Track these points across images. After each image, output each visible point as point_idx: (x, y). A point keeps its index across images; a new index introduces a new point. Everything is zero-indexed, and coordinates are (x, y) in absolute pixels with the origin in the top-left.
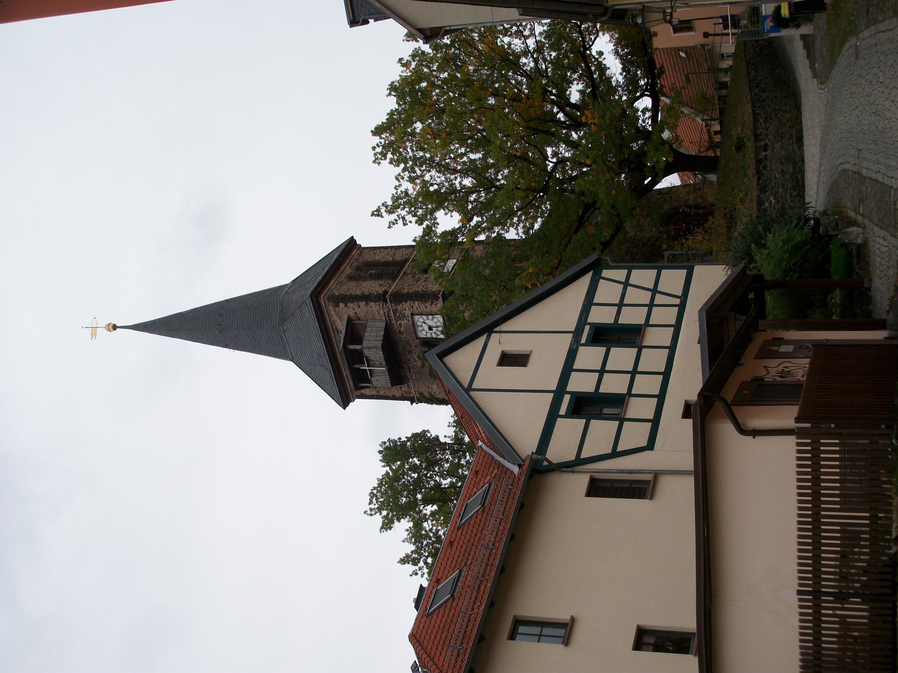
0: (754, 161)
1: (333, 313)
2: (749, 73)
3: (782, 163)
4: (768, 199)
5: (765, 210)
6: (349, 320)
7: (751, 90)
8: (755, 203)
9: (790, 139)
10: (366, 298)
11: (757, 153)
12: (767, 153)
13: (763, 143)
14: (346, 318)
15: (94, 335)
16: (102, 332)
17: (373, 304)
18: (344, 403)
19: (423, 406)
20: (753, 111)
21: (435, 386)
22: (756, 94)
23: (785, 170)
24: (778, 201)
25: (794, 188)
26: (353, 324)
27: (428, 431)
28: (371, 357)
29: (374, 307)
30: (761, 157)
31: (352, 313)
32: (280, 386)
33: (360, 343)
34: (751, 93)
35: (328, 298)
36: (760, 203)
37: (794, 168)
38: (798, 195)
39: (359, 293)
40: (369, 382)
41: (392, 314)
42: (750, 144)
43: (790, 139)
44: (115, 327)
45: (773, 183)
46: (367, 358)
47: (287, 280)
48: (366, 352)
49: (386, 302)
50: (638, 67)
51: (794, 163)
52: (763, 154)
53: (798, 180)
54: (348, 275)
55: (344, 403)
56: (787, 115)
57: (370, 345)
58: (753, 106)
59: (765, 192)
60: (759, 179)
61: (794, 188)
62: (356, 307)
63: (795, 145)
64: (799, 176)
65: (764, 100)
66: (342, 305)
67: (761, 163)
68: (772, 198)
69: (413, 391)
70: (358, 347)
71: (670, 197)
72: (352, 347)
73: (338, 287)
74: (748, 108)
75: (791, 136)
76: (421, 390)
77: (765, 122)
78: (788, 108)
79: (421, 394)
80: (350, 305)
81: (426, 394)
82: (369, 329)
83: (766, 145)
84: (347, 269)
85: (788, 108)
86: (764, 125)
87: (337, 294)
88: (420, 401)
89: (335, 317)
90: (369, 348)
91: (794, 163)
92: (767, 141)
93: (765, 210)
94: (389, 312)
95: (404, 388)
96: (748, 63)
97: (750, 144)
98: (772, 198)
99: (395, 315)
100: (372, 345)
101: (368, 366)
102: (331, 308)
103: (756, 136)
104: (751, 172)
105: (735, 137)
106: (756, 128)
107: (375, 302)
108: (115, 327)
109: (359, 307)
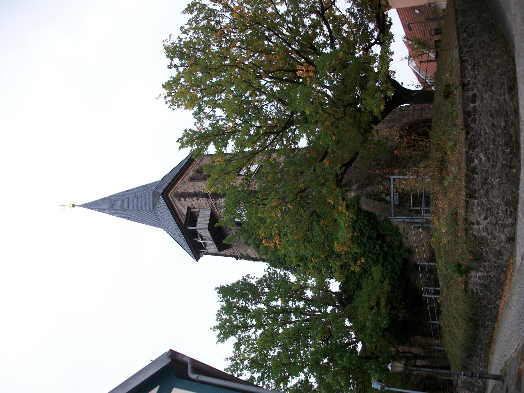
0: (462, 114)
1: (178, 204)
2: (457, 19)
3: (492, 115)
4: (478, 156)
5: (475, 168)
6: (189, 208)
7: (458, 35)
8: (464, 157)
9: (500, 89)
10: (197, 195)
11: (465, 105)
12: (476, 104)
13: (471, 93)
17: (201, 199)
20: (461, 58)
21: (249, 250)
22: (464, 39)
24: (488, 158)
25: (507, 144)
26: (192, 212)
28: (203, 235)
31: (190, 205)
32: (159, 243)
33: (195, 225)
34: (458, 38)
35: (174, 195)
36: (469, 160)
37: (506, 122)
38: (511, 152)
39: (193, 191)
40: (205, 249)
41: (214, 205)
42: (457, 93)
44: (74, 206)
45: (482, 139)
46: (200, 235)
48: (199, 232)
49: (209, 198)
51: (507, 115)
52: (472, 105)
53: (511, 135)
54: (190, 177)
56: (497, 61)
57: (201, 227)
58: (460, 53)
60: (467, 133)
61: (507, 144)
62: (191, 201)
63: (507, 95)
64: (512, 131)
66: (183, 199)
67: (469, 116)
68: (481, 155)
70: (194, 228)
71: (408, 113)
72: (190, 228)
73: (182, 187)
74: (455, 54)
75: (502, 84)
76: (241, 252)
77: (473, 69)
78: (497, 53)
81: (244, 254)
82: (200, 216)
83: (475, 95)
84: (191, 172)
85: (497, 53)
86: (471, 73)
87: (180, 192)
88: (241, 258)
89: (180, 207)
90: (200, 229)
91: (507, 115)
92: (476, 91)
93: (475, 168)
94: (212, 204)
95: (231, 250)
96: (456, 10)
97: (457, 93)
98: (481, 155)
99: (216, 206)
101: (202, 240)
103: (464, 85)
104: (460, 121)
108: (74, 206)
109: (193, 200)
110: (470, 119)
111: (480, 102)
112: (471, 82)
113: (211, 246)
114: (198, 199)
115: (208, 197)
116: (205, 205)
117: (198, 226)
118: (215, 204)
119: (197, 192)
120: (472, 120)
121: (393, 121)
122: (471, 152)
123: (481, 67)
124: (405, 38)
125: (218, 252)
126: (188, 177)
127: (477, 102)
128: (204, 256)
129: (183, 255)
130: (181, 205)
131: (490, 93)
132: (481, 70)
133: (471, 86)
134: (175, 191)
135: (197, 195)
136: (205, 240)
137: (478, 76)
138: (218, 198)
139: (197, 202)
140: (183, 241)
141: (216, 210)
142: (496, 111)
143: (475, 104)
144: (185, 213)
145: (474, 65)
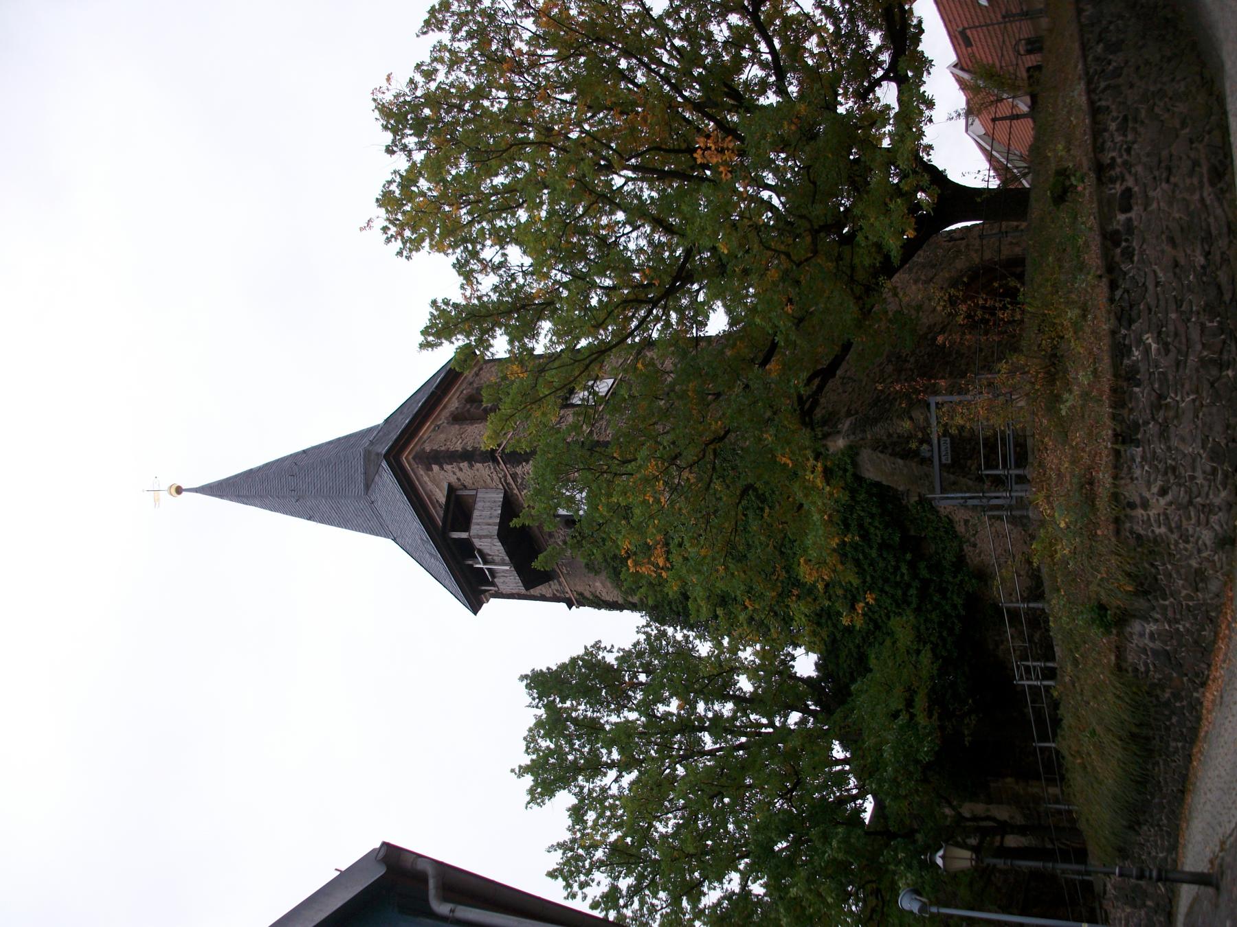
0: (1098, 239)
1: (426, 479)
2: (1079, 12)
3: (1172, 241)
4: (1140, 341)
6: (451, 489)
7: (1084, 48)
8: (1105, 344)
9: (1191, 173)
10: (469, 456)
11: (1105, 218)
12: (1132, 214)
13: (1118, 188)
14: (446, 486)
15: (157, 501)
16: (165, 496)
17: (479, 465)
18: (475, 607)
19: (586, 611)
20: (1091, 102)
21: (598, 584)
22: (1097, 59)
23: (1182, 261)
26: (458, 497)
27: (597, 646)
28: (486, 550)
29: (483, 470)
30: (1115, 226)
31: (453, 480)
32: (381, 573)
33: (466, 529)
34: (1085, 57)
35: (414, 458)
36: (1120, 351)
37: (1207, 254)
39: (459, 447)
41: (510, 479)
42: (1085, 188)
43: (1191, 173)
44: (179, 490)
46: (480, 552)
47: (379, 420)
48: (477, 543)
49: (498, 463)
50: (871, 26)
52: (1122, 217)
53: (1219, 287)
55: (475, 607)
56: (1181, 108)
57: (481, 533)
58: (1090, 91)
59: (1131, 322)
60: (1113, 286)
62: (457, 470)
63: (1207, 190)
65: (1117, 73)
66: (436, 468)
67: (1117, 244)
68: (1149, 339)
69: (567, 589)
70: (464, 535)
71: (967, 246)
72: (456, 535)
73: (435, 437)
74: (1078, 94)
75: (1196, 163)
76: (580, 589)
77: (1123, 129)
79: (581, 594)
80: (447, 467)
81: (587, 594)
82: (479, 505)
83: (1128, 193)
84: (453, 402)
86: (1118, 139)
87: (428, 449)
88: (581, 604)
89: (430, 486)
90: (480, 537)
92: (1130, 182)
94: (505, 476)
95: (554, 585)
97: (1085, 188)
98: (1149, 339)
99: (515, 481)
100: (484, 531)
101: (485, 562)
102: (422, 472)
103: (1100, 169)
104: (1093, 258)
105: (1053, 166)
106: (1098, 148)
107: (483, 462)
108: (179, 490)
109: (461, 470)
110: (1118, 251)
111: (1141, 208)
112: (1119, 161)
113: (507, 576)
114: (471, 466)
115: (495, 460)
116: (489, 480)
117: (474, 529)
118: (514, 476)
119: (469, 448)
120: (1123, 253)
121: (933, 266)
122: (1123, 331)
123: (1142, 122)
124: (955, 66)
125: (523, 591)
126: (446, 413)
127: (1135, 208)
128: (492, 600)
129: (440, 599)
130: (433, 481)
131: (1164, 186)
132: (1141, 130)
133: (1118, 170)
134: (418, 448)
135: (469, 456)
136: (493, 562)
137: (1136, 146)
138: (520, 463)
139: (469, 472)
140: (441, 567)
141: (516, 491)
142: (1182, 229)
143: (1128, 215)
144: (443, 500)
145: (1125, 118)
